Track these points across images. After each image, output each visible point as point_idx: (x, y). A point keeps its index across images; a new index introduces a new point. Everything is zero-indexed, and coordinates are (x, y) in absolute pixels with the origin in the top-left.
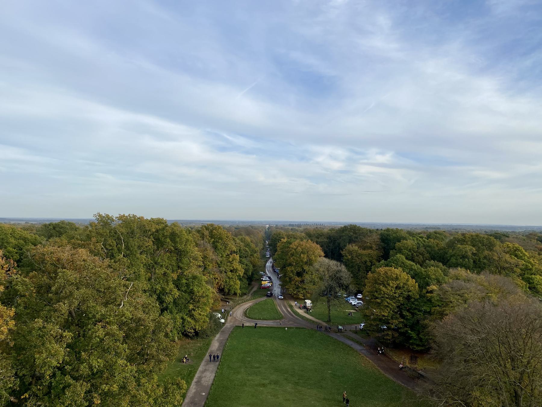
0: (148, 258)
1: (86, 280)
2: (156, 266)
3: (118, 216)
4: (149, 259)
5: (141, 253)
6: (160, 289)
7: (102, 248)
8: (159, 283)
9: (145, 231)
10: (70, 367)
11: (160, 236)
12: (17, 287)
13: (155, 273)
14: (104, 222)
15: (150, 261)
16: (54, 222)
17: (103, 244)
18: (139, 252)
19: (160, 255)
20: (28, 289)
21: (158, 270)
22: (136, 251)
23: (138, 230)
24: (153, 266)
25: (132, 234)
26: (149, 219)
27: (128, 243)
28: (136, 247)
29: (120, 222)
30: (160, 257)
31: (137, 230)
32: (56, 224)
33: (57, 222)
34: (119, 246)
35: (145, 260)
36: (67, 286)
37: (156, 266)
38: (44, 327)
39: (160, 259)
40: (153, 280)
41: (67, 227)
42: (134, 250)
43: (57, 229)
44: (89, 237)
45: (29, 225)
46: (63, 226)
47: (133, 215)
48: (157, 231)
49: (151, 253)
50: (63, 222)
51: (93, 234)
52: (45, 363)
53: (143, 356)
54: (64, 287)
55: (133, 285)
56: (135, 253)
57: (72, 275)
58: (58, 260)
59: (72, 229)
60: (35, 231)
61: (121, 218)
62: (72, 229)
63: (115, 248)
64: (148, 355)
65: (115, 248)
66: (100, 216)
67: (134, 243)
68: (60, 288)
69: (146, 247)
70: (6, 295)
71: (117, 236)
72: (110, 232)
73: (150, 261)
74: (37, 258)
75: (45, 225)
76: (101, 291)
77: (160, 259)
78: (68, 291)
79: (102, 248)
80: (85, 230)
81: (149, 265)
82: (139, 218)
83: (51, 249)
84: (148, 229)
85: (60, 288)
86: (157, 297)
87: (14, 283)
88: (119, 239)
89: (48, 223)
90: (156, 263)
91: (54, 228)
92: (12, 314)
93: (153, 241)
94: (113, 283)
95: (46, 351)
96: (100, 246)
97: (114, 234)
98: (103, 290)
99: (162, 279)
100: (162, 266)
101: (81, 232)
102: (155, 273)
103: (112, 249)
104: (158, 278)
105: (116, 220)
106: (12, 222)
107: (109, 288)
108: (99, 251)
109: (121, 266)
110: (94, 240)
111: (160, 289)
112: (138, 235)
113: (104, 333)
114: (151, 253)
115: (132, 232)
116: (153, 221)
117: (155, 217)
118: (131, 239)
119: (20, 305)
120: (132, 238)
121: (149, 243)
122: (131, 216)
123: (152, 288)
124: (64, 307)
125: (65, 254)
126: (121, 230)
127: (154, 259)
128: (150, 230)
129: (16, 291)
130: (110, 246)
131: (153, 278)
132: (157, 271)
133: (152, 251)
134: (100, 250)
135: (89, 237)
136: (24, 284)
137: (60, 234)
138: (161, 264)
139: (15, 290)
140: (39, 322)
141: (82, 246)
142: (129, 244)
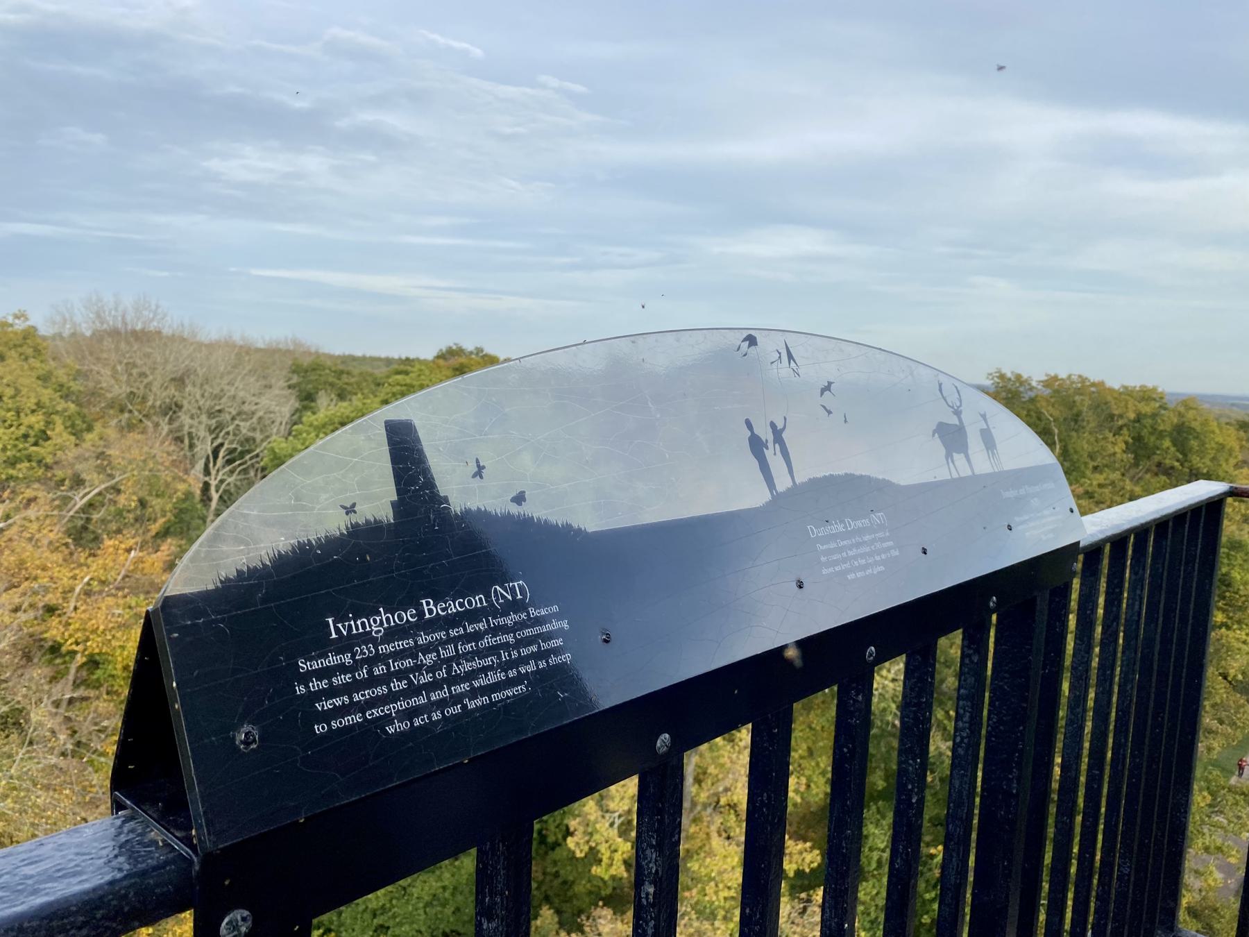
9: (1111, 417)
11: (1145, 432)
14: (1009, 391)
22: (1086, 464)
26: (1116, 386)
31: (1087, 414)
47: (1080, 376)
56: (1083, 467)
61: (1050, 382)
66: (1002, 376)
71: (1042, 424)
82: (1093, 385)
93: (1126, 443)
115: (1076, 418)
117: (1134, 382)
118: (1074, 434)
120: (1076, 431)
122: (1074, 378)
128: (1121, 416)
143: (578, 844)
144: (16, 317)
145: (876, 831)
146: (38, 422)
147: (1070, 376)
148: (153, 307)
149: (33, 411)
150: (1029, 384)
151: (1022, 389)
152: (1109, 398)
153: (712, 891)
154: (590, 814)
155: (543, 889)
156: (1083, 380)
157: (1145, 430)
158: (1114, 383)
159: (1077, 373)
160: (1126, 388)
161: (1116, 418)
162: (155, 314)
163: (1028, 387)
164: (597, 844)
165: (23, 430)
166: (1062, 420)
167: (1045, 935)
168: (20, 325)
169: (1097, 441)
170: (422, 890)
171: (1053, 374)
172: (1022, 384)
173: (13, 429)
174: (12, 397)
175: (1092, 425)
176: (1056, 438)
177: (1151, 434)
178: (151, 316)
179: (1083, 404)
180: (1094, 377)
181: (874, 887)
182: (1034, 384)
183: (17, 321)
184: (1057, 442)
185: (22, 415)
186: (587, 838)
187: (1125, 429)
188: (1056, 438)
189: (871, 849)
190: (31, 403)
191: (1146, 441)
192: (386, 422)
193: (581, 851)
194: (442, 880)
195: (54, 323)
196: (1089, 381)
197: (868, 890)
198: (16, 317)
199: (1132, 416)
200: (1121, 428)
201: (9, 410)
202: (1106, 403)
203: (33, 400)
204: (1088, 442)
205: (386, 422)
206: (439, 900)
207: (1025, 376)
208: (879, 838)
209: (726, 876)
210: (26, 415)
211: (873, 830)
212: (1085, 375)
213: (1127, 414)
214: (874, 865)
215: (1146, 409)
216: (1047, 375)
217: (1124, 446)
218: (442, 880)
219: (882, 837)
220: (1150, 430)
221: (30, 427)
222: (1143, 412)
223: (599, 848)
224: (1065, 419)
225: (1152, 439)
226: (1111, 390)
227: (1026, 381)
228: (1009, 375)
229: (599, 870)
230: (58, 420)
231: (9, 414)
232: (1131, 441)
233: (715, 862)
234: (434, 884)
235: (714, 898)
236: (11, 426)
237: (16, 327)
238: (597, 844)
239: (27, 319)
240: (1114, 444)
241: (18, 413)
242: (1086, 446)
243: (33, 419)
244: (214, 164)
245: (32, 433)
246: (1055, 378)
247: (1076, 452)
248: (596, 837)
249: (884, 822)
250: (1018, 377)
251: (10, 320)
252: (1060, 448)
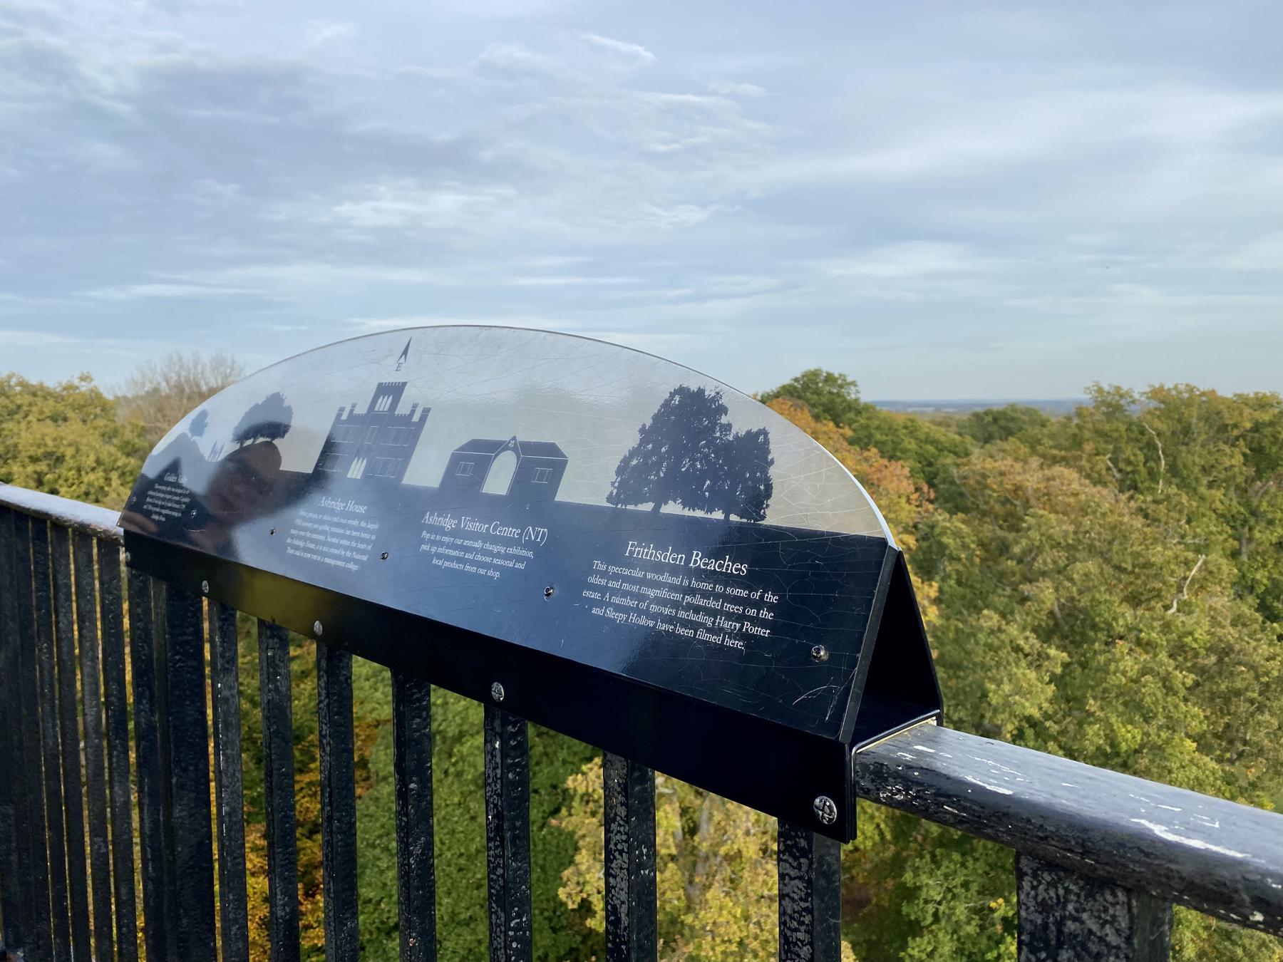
0: (1231, 500)
1: (1089, 538)
2: (1252, 521)
3: (1148, 390)
4: (1234, 503)
5: (1211, 485)
6: (1265, 581)
7: (1109, 469)
8: (1264, 566)
9: (1224, 428)
10: (1056, 727)
11: (1265, 442)
12: (945, 540)
13: (1250, 540)
14: (1109, 405)
15: (1237, 508)
16: (995, 409)
17: (1110, 459)
18: (1205, 482)
19: (1266, 493)
20: (965, 547)
21: (1260, 532)
22: (1197, 480)
23: (1201, 424)
24: (1245, 521)
25: (1186, 435)
26: (1229, 395)
27: (1175, 458)
28: (1196, 470)
29: (1153, 404)
30: (1267, 498)
31: (1197, 425)
32: (998, 412)
33: (1000, 409)
34: (1152, 464)
35: (1222, 502)
36: (1047, 548)
37: (1252, 521)
38: (1000, 630)
39: (1265, 504)
40: (1244, 558)
41: (1023, 417)
42: (1192, 476)
43: (1002, 423)
44: (1077, 442)
45: (942, 415)
46: (1014, 415)
47: (1187, 385)
48: (1257, 428)
49: (1238, 487)
50: (1013, 407)
51: (1087, 434)
52: (1007, 705)
53: (1231, 742)
54: (1040, 549)
55: (1205, 563)
56: (1194, 484)
57: (1060, 527)
58: (1018, 488)
59: (1033, 422)
60: (954, 428)
61: (1157, 393)
62: (1033, 422)
63: (1141, 468)
64: (1245, 743)
65: (1141, 468)
66: (1100, 390)
67: (1193, 457)
68: (1030, 551)
69: (1226, 469)
70: (924, 553)
71: (1145, 439)
72: (1127, 430)
73: (1237, 508)
74: (972, 482)
75: (976, 415)
76: (1125, 569)
77: (1265, 504)
78: (1049, 561)
79: (1109, 469)
80: (1065, 426)
81: (1233, 516)
82: (1203, 394)
83: (1002, 465)
84: (1231, 422)
85: (1030, 551)
86: (1258, 601)
87: (937, 530)
88: (1151, 446)
89: (980, 410)
90: (1253, 513)
91: (995, 420)
92: (933, 593)
93: (1244, 455)
94: (1158, 554)
95: (1010, 681)
96: (1104, 461)
97: (1138, 432)
98: (1130, 568)
99: (1271, 557)
100: (1271, 522)
101: (1055, 429)
102: (1250, 540)
103: (1133, 472)
104: (1258, 553)
105: (1143, 399)
106: (910, 410)
107: (1147, 565)
108: (1100, 475)
109: (1172, 514)
110: (1088, 447)
111: (1265, 581)
112: (1201, 438)
113: (1136, 667)
114: (1238, 487)
115: (1187, 431)
116: (1243, 401)
117: (1249, 391)
118: (1184, 448)
119: (949, 577)
120: (1187, 444)
121: (1234, 459)
122: (1182, 387)
123: (1244, 576)
124: (1046, 594)
125: (1031, 477)
126: (1157, 424)
127: (1247, 505)
128: (1235, 426)
129: (943, 547)
130: (1129, 463)
131: (1244, 550)
132: (1257, 535)
133: (1240, 480)
134: (1104, 472)
135: (1077, 442)
136: (957, 534)
137: (1008, 433)
138: (1270, 516)
139: (940, 544)
140: (990, 619)
141: (1064, 461)
142: (1179, 463)
143: (569, 895)
144: (82, 379)
145: (931, 882)
146: (98, 479)
147: (1176, 387)
148: (229, 362)
149: (93, 469)
150: (1131, 397)
151: (1122, 402)
152: (1221, 407)
153: (708, 946)
154: (582, 863)
155: (590, 943)
156: (1191, 389)
157: (1265, 440)
158: (1226, 391)
159: (1184, 382)
160: (1240, 396)
161: (1229, 428)
162: (232, 369)
163: (1129, 400)
164: (589, 895)
165: (83, 488)
166: (1168, 434)
167: (97, 960)
168: (84, 387)
169: (1210, 453)
170: (457, 944)
171: (1157, 386)
172: (1122, 396)
173: (74, 487)
174: (73, 457)
175: (1203, 437)
176: (1160, 452)
177: (1273, 443)
178: (228, 371)
179: (1193, 415)
180: (1203, 386)
181: (929, 943)
182: (1136, 396)
183: (83, 383)
184: (1162, 456)
185: (83, 473)
186: (579, 889)
187: (1241, 440)
188: (1160, 452)
189: (926, 902)
190: (91, 461)
191: (1267, 451)
192: (764, 432)
193: (573, 902)
194: (476, 934)
195: (136, 383)
196: (1198, 390)
197: (923, 947)
198: (82, 379)
199: (1248, 425)
200: (1237, 438)
201: (70, 469)
202: (1218, 413)
203: (92, 458)
204: (1200, 456)
205: (764, 432)
206: (474, 954)
207: (1125, 388)
208: (934, 890)
209: (722, 930)
210: (87, 473)
211: (926, 881)
212: (1193, 384)
213: (1244, 424)
214: (930, 919)
215: (1266, 417)
216: (1150, 386)
217: (1242, 459)
218: (476, 934)
219: (939, 889)
220: (1272, 439)
221: (90, 484)
222: (1261, 421)
223: (591, 899)
224: (1173, 433)
225: (1274, 449)
226: (1224, 400)
227: (1127, 392)
228: (1106, 388)
229: (593, 923)
230: (114, 476)
231: (70, 474)
232: (1248, 451)
233: (709, 915)
234: (469, 938)
235: (711, 953)
236: (73, 484)
237: (83, 389)
238: (589, 895)
239: (92, 380)
240: (1232, 456)
241: (79, 470)
242: (1197, 460)
243: (92, 477)
244: (346, 209)
245: (92, 491)
246: (1161, 388)
247: (1185, 467)
248: (588, 888)
249: (939, 872)
250: (1118, 389)
251: (76, 382)
252: (1166, 464)
